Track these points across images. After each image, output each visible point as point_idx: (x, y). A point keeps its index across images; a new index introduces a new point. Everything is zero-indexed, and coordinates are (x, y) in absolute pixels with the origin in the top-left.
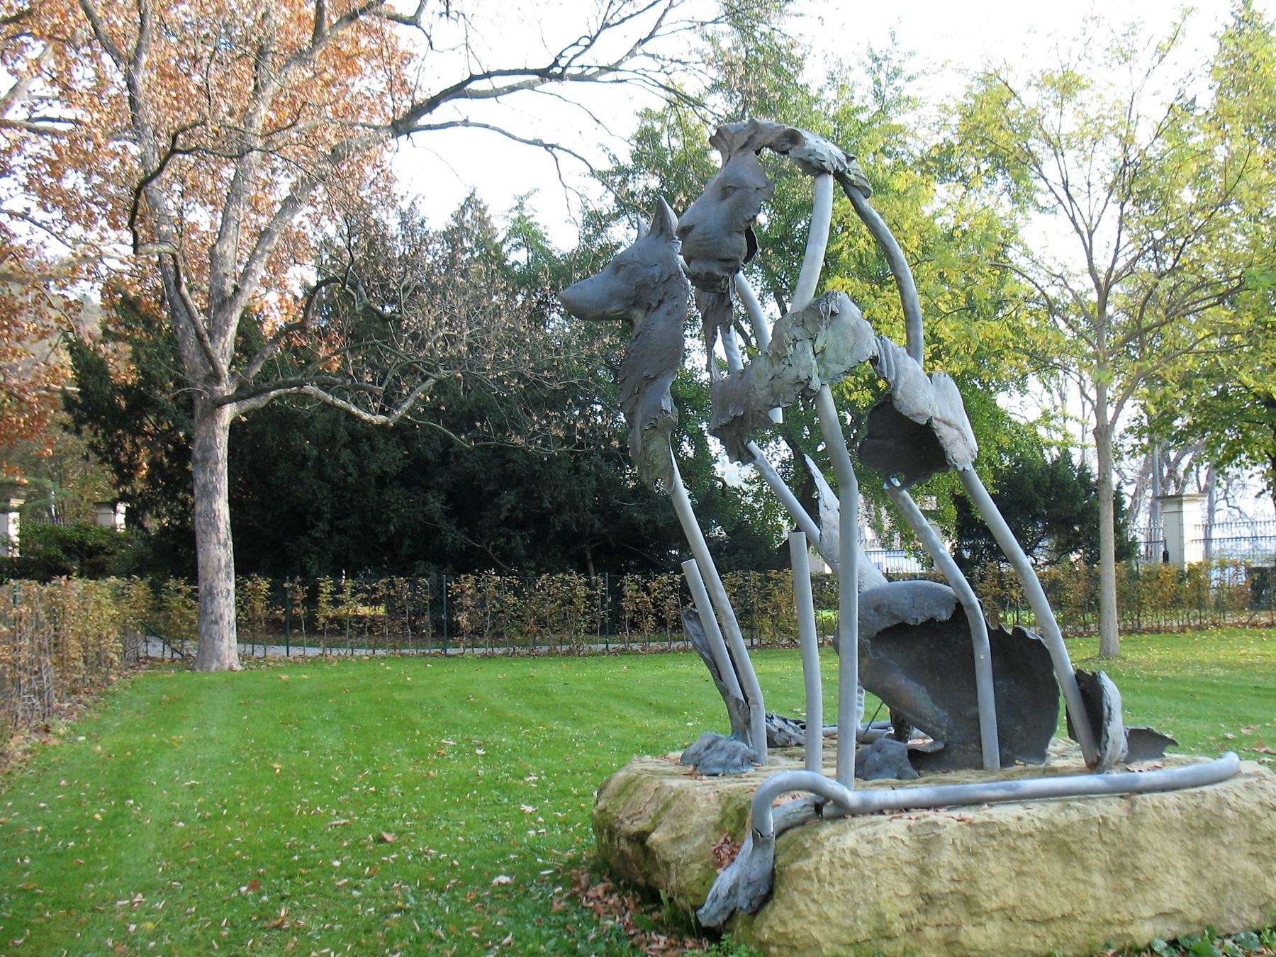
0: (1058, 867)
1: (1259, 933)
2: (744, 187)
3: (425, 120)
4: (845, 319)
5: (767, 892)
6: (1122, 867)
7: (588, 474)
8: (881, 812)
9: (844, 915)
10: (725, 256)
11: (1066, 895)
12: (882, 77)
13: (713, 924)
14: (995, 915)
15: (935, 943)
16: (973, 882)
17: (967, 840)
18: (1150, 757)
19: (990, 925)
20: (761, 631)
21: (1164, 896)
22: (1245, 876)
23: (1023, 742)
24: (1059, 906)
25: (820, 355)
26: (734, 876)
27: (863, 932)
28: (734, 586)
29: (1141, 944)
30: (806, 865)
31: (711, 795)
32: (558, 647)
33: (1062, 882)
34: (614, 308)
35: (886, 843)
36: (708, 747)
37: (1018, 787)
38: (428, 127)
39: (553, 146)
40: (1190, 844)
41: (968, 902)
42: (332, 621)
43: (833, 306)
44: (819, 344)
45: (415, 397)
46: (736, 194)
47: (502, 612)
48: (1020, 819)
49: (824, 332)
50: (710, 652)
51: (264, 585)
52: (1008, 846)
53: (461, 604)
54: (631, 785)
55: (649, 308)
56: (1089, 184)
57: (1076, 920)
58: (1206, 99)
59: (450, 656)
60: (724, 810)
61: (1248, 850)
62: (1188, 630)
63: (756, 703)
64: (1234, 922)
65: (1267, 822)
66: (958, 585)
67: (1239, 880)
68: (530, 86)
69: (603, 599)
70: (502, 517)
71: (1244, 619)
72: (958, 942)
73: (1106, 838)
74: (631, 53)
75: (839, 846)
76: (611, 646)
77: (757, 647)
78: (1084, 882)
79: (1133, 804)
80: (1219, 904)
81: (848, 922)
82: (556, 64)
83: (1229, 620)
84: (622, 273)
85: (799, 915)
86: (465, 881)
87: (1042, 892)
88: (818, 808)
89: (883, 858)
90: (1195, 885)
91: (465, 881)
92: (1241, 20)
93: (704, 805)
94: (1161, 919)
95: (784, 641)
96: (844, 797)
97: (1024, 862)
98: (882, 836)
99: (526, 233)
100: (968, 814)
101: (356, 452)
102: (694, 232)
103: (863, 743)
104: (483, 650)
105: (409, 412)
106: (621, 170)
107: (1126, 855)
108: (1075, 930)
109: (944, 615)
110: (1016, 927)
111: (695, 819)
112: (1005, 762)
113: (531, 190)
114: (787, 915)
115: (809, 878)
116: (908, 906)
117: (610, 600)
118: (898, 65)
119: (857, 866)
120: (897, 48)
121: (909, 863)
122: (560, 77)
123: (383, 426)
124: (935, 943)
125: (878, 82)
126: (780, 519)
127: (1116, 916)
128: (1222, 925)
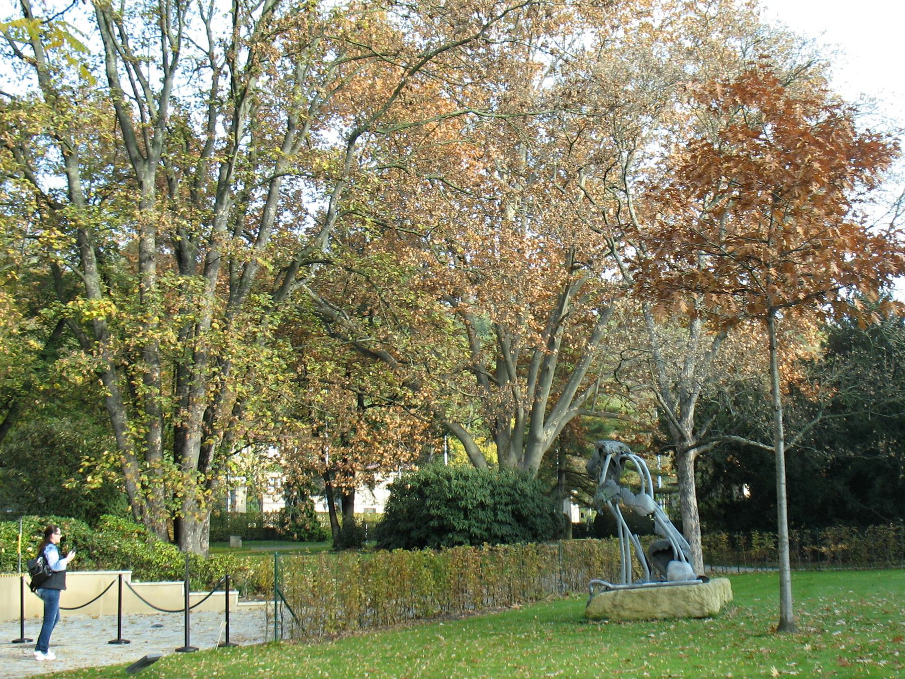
24: (640, 608)
41: (622, 606)
51: (724, 536)
109: (666, 548)
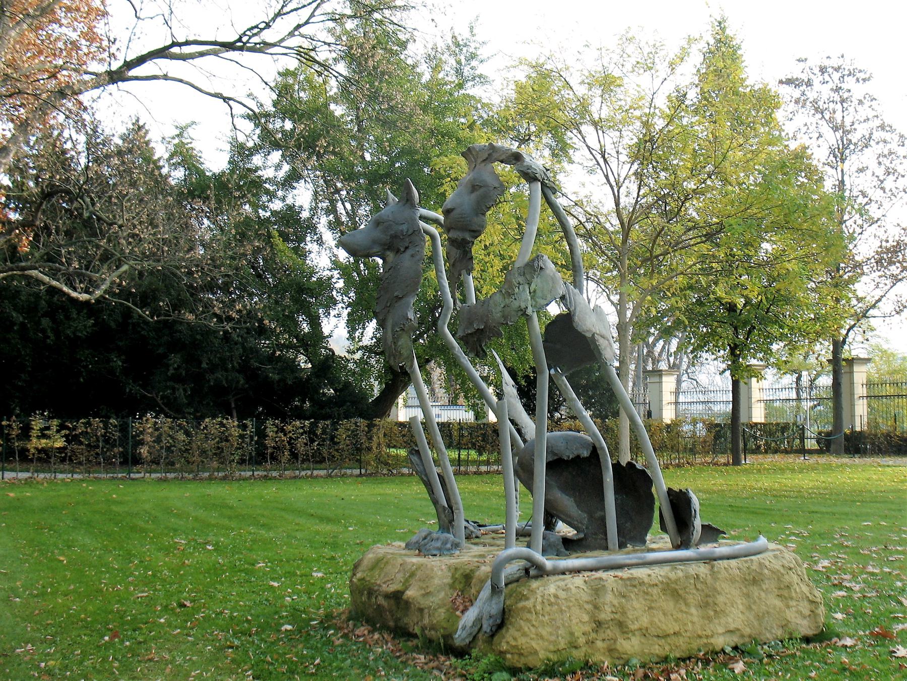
0: (671, 604)
1: (782, 642)
2: (486, 186)
3: (133, 73)
4: (548, 272)
5: (502, 622)
6: (707, 605)
7: (236, 344)
8: (564, 573)
9: (551, 634)
10: (474, 228)
11: (676, 620)
12: (462, 58)
13: (463, 644)
14: (636, 633)
15: (602, 650)
16: (624, 613)
17: (620, 588)
18: (710, 542)
19: (633, 639)
20: (368, 463)
21: (730, 620)
22: (774, 608)
23: (633, 532)
25: (533, 294)
26: (476, 614)
27: (562, 644)
28: (348, 430)
29: (718, 649)
30: (529, 604)
31: (443, 567)
32: (216, 474)
33: (674, 613)
34: (375, 250)
35: (574, 590)
36: (425, 538)
37: (645, 557)
38: (137, 78)
39: (230, 99)
40: (745, 590)
41: (621, 625)
42: (40, 451)
43: (541, 264)
44: (533, 287)
45: (108, 279)
46: (482, 190)
47: (174, 446)
48: (649, 575)
49: (535, 279)
50: (426, 475)
52: (644, 592)
53: (143, 439)
54: (378, 563)
55: (398, 251)
56: (617, 152)
57: (681, 635)
58: (692, 96)
59: (133, 479)
60: (453, 576)
61: (776, 593)
62: (671, 467)
63: (458, 509)
64: (768, 635)
65: (786, 577)
66: (594, 435)
67: (771, 611)
68: (216, 53)
69: (252, 438)
70: (169, 374)
71: (708, 459)
72: (616, 649)
73: (699, 586)
74: (291, 34)
75: (546, 592)
76: (256, 473)
77: (364, 475)
78: (686, 612)
79: (713, 567)
80: (760, 625)
81: (553, 638)
82: (240, 40)
83: (698, 461)
84: (380, 227)
85: (524, 635)
86: (262, 629)
87: (663, 619)
88: (527, 571)
89: (573, 599)
90: (747, 614)
91: (262, 629)
92: (720, 41)
93: (440, 573)
94: (728, 635)
95: (385, 471)
96: (544, 564)
97: (652, 601)
98: (570, 586)
99: (184, 156)
100: (619, 573)
101: (54, 320)
102: (452, 214)
103: (521, 536)
104: (159, 475)
105: (105, 292)
106: (267, 115)
107: (709, 596)
108: (681, 641)
109: (585, 454)
110: (648, 640)
111: (436, 581)
112: (622, 545)
113: (189, 122)
114: (517, 634)
115: (530, 612)
116: (587, 628)
117: (256, 438)
118: (474, 51)
119: (558, 604)
120: (474, 38)
121: (587, 602)
122: (241, 49)
123: (87, 302)
124: (602, 650)
125: (459, 62)
126: (372, 380)
127: (704, 633)
128: (762, 637)
